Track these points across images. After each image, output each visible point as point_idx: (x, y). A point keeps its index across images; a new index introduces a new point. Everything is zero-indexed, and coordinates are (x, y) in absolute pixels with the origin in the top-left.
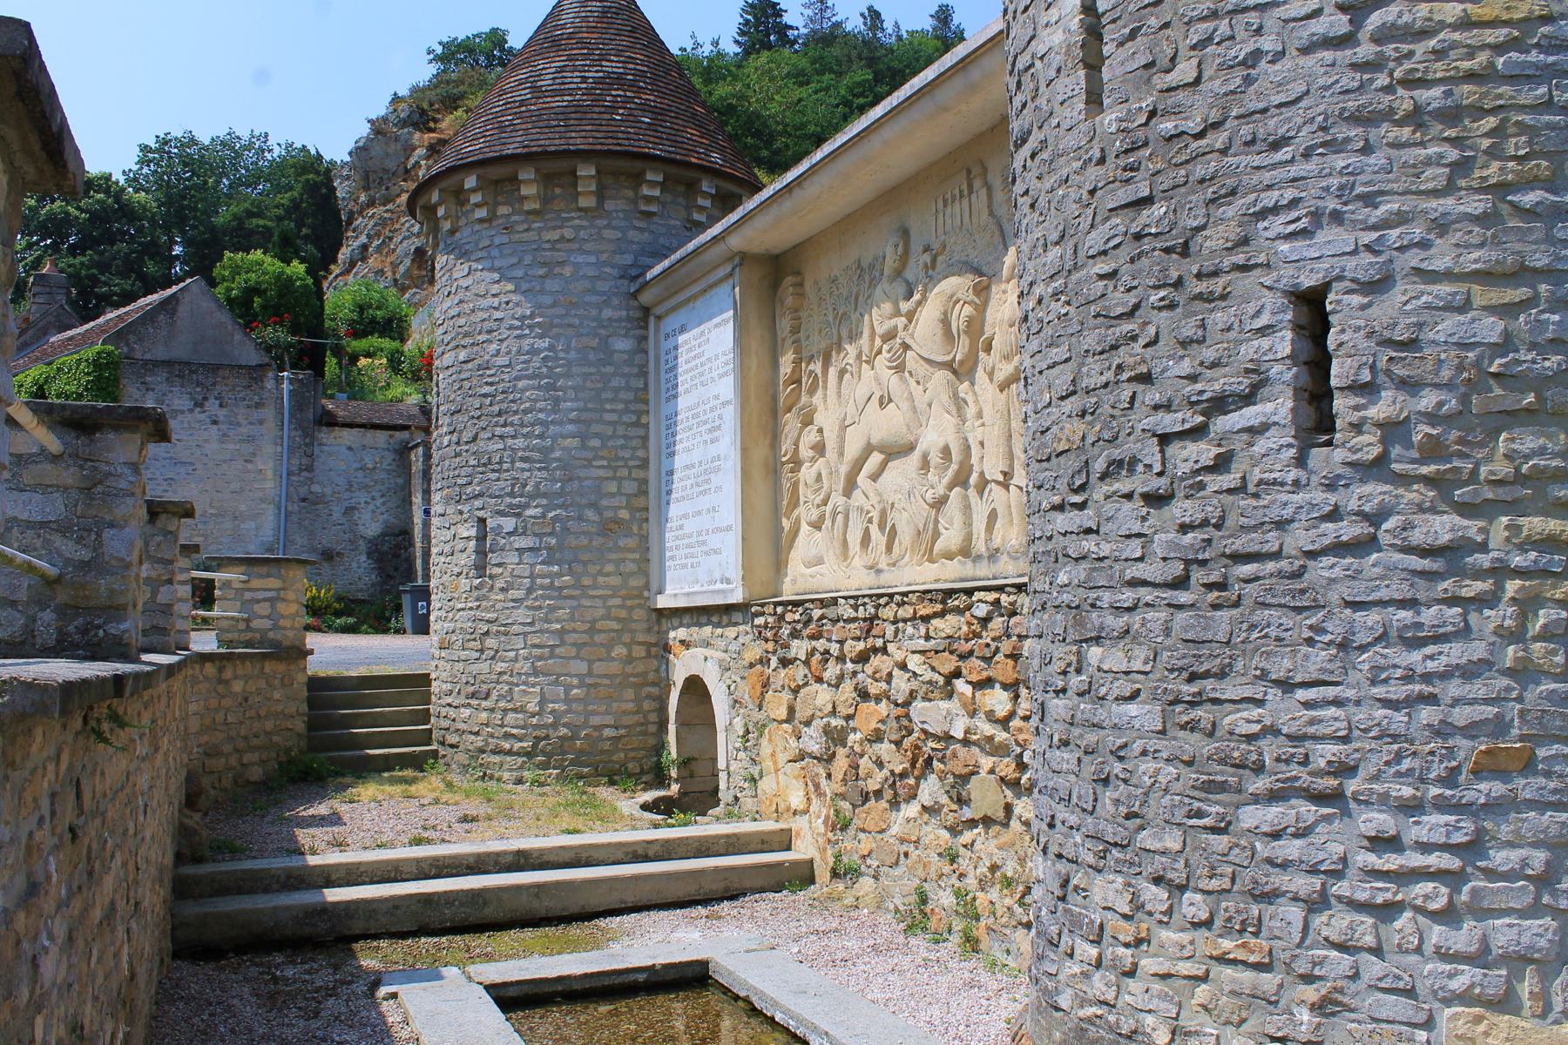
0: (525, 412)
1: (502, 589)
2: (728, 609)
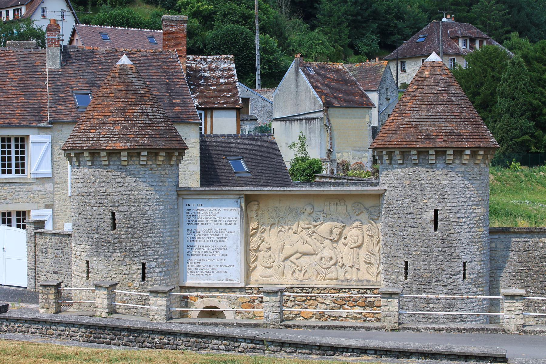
0: (158, 229)
1: (152, 285)
2: (241, 288)
